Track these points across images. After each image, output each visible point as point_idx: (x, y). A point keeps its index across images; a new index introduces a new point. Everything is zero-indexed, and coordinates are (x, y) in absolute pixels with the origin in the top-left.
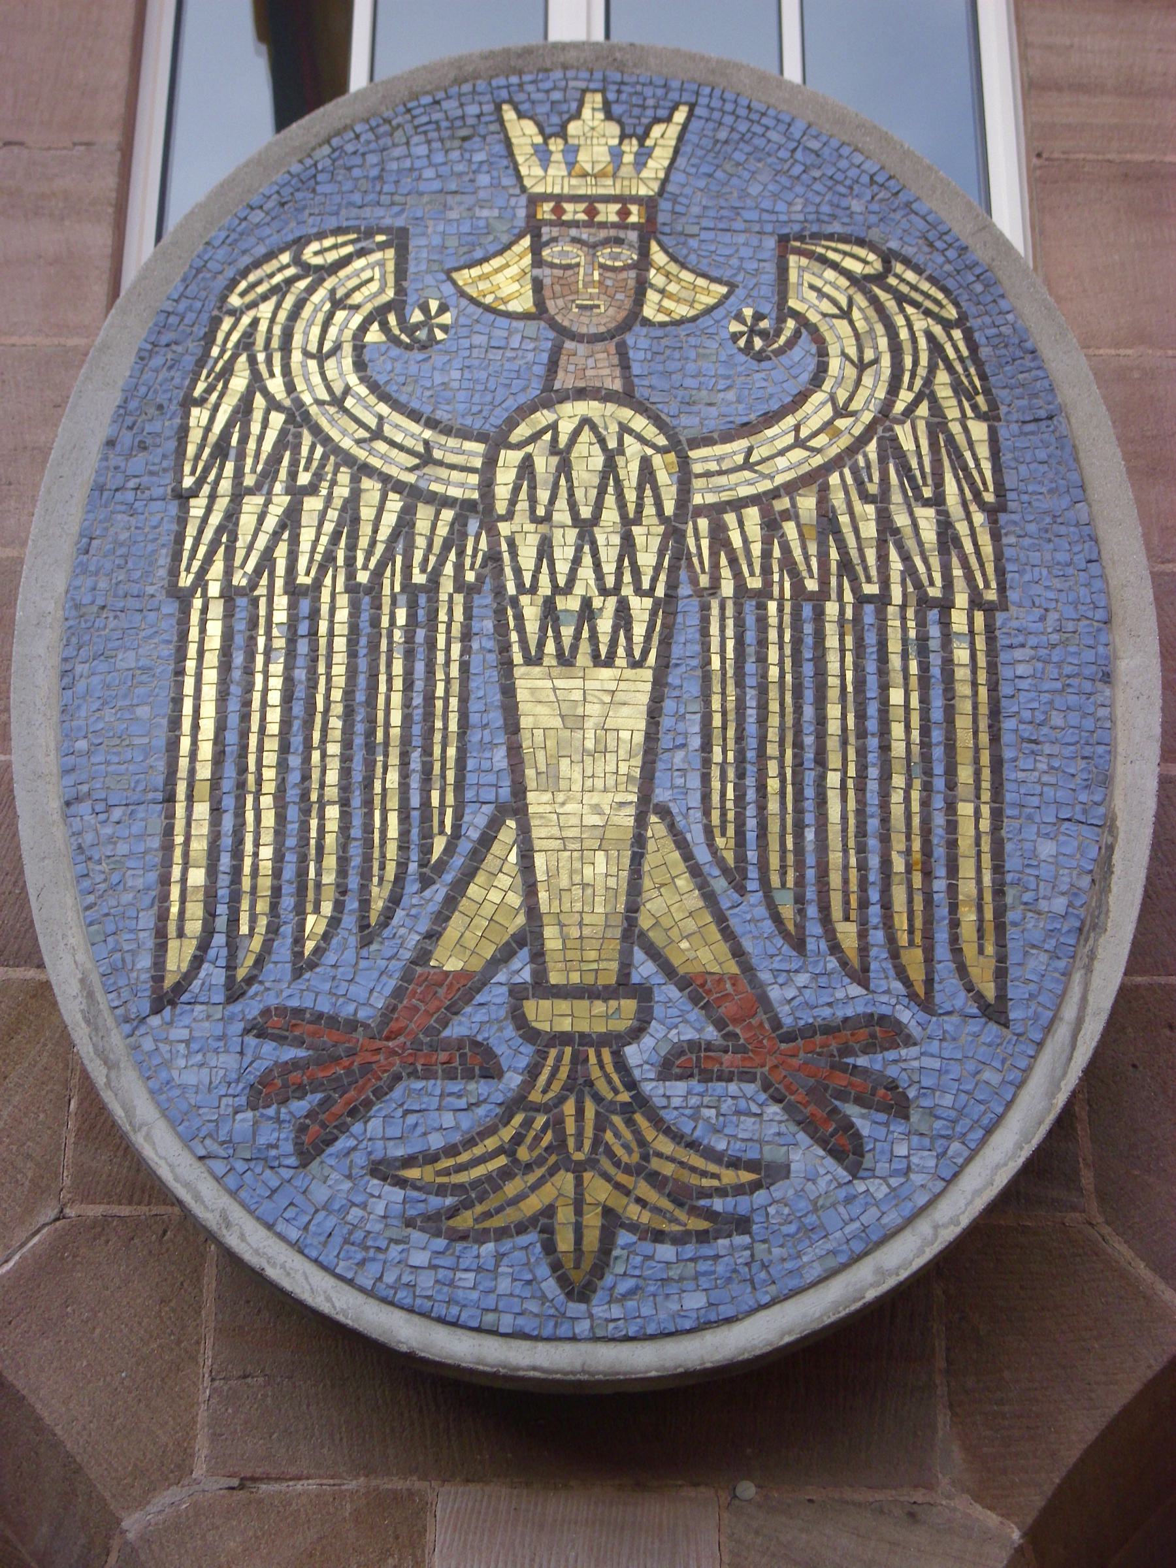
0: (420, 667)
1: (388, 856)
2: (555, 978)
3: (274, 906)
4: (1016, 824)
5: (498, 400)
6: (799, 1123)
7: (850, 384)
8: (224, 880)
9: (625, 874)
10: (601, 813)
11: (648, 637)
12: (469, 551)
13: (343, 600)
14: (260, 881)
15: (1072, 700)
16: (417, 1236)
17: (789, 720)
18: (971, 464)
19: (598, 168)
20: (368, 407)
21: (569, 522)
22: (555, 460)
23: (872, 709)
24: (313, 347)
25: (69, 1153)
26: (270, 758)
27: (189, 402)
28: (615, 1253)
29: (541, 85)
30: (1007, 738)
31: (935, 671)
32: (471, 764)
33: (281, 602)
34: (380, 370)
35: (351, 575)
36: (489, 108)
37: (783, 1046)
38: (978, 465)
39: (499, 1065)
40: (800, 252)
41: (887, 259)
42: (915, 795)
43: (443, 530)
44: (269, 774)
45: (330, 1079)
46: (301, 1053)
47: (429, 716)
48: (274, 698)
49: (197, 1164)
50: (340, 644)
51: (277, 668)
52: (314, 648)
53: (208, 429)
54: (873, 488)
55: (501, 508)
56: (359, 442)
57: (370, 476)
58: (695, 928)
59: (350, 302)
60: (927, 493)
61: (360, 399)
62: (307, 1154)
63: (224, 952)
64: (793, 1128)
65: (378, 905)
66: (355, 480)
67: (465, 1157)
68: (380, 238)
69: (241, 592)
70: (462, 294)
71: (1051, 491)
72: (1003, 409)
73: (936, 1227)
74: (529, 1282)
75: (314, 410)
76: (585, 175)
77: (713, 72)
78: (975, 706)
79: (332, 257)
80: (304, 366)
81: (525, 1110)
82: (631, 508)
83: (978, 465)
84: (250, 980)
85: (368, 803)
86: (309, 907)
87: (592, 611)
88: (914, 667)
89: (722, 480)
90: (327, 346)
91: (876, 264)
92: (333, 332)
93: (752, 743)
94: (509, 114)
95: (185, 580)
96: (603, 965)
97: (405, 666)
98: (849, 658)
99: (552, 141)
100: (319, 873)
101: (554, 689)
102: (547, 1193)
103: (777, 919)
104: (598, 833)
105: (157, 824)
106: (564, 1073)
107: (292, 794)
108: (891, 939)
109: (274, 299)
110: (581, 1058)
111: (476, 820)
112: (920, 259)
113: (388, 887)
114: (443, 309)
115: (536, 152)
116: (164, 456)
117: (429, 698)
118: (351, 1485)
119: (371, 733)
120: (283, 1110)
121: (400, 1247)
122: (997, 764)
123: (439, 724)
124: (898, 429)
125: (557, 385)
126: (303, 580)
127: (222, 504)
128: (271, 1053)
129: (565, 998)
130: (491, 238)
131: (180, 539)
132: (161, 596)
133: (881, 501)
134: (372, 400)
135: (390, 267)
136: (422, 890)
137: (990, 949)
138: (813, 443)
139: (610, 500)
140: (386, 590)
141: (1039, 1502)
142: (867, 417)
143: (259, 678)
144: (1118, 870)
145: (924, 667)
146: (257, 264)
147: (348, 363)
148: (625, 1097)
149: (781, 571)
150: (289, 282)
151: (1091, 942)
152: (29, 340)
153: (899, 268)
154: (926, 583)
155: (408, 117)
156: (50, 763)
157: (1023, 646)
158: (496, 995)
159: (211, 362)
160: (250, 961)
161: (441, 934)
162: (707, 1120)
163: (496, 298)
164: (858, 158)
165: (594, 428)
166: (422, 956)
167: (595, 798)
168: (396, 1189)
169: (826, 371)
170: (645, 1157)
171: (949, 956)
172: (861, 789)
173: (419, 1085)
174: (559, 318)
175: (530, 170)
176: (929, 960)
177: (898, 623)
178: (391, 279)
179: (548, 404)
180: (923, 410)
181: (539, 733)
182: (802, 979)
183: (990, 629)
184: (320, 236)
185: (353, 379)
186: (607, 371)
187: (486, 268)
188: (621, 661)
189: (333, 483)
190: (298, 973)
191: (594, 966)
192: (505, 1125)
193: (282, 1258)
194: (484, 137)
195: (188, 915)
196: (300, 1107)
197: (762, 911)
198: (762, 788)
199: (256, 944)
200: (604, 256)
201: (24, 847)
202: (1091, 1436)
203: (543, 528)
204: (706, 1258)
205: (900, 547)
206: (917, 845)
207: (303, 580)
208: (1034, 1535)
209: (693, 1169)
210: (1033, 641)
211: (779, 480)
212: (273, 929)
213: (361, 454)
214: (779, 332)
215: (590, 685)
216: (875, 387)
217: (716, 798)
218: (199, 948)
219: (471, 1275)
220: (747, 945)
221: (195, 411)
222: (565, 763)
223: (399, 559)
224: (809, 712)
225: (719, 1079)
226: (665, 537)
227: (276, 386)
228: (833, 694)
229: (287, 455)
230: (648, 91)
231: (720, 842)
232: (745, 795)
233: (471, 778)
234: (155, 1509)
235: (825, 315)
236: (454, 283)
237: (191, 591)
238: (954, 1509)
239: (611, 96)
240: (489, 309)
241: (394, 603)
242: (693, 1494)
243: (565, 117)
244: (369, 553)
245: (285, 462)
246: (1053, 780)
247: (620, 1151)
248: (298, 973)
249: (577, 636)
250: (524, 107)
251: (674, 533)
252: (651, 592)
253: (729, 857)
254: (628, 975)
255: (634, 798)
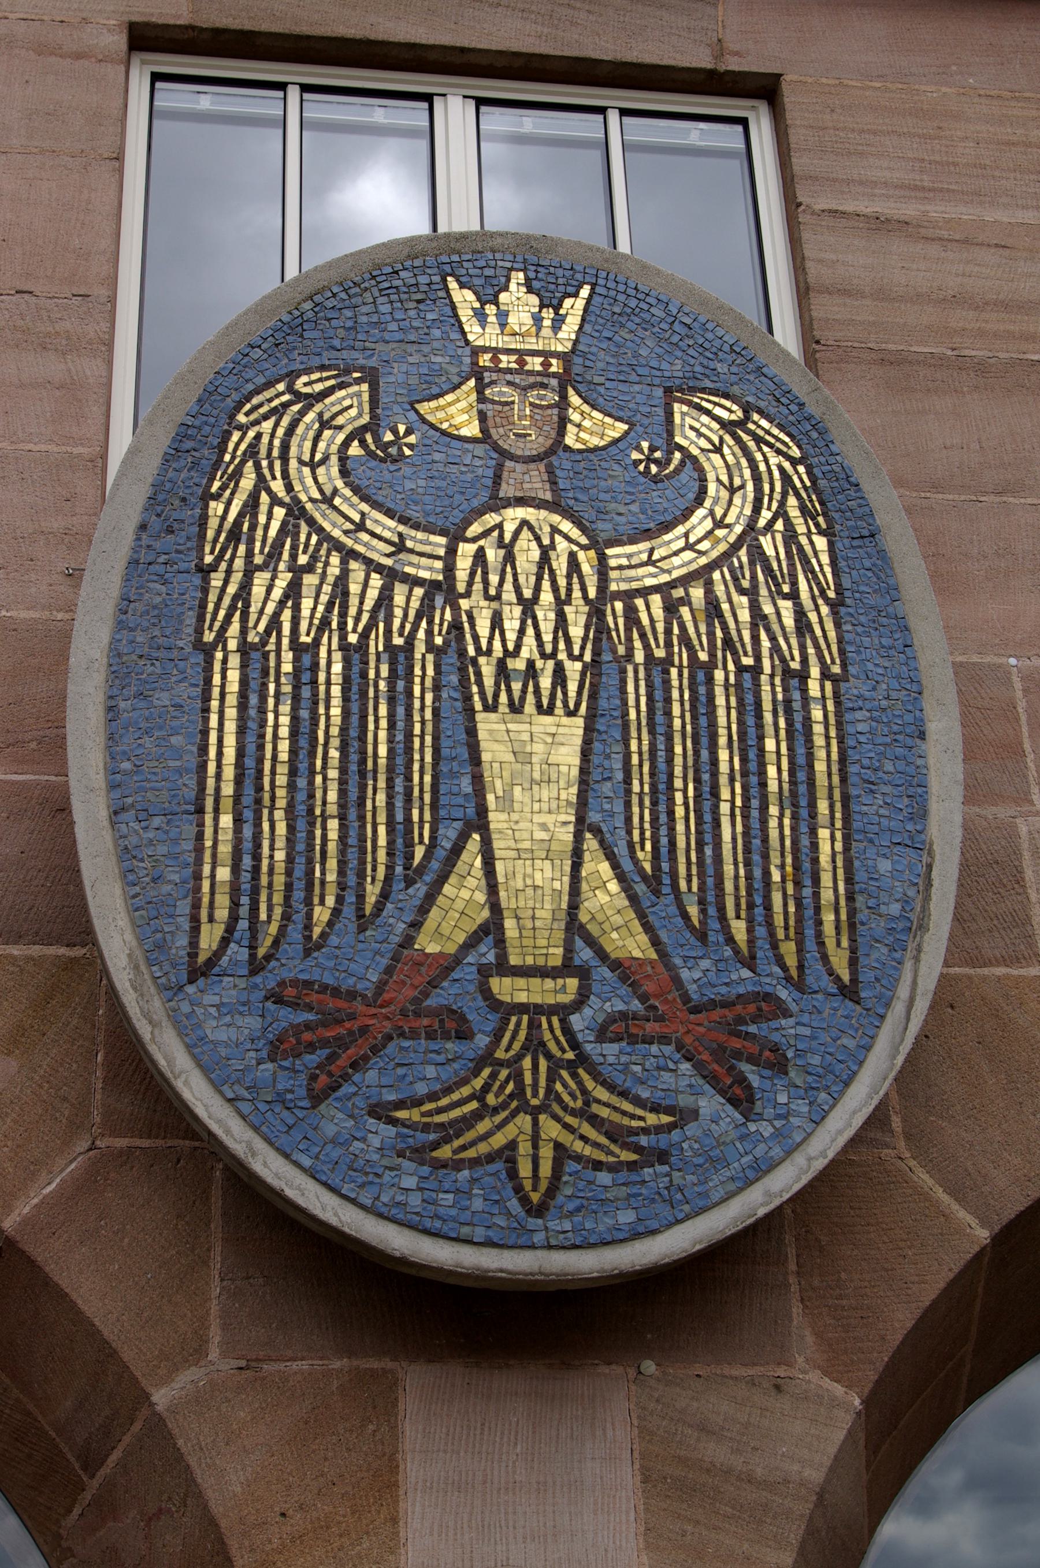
0: (401, 711)
1: (379, 860)
2: (514, 960)
3: (287, 898)
4: (861, 845)
5: (456, 503)
6: (704, 1077)
7: (724, 502)
8: (246, 877)
9: (566, 879)
10: (547, 830)
11: (580, 693)
12: (437, 621)
13: (337, 656)
14: (276, 878)
15: (899, 751)
16: (406, 1164)
17: (690, 762)
18: (817, 568)
19: (524, 329)
20: (352, 506)
21: (515, 601)
22: (502, 552)
23: (752, 755)
24: (306, 457)
25: (98, 1096)
26: (282, 780)
27: (207, 497)
28: (565, 1178)
29: (476, 263)
30: (853, 779)
31: (798, 726)
32: (443, 788)
33: (288, 656)
34: (360, 474)
35: (343, 637)
36: (437, 279)
37: (692, 1016)
38: (822, 570)
39: (470, 1029)
40: (682, 402)
41: (747, 409)
42: (787, 822)
43: (415, 604)
44: (281, 793)
45: (335, 1038)
46: (310, 1017)
47: (409, 750)
48: (284, 732)
49: (227, 1105)
50: (336, 691)
51: (285, 708)
52: (315, 694)
53: (223, 518)
54: (746, 584)
55: (461, 588)
56: (346, 532)
57: (356, 560)
58: (622, 922)
59: (334, 423)
60: (786, 589)
61: (346, 499)
62: (317, 1099)
63: (248, 934)
64: (701, 1082)
65: (371, 899)
66: (344, 562)
67: (444, 1102)
68: (356, 375)
69: (254, 647)
70: (424, 421)
71: (875, 591)
72: (838, 527)
73: (810, 1159)
74: (497, 1202)
75: (309, 506)
76: (515, 334)
77: (607, 261)
78: (829, 755)
79: (318, 387)
80: (300, 472)
81: (491, 1065)
82: (563, 592)
83: (822, 570)
84: (268, 958)
85: (362, 818)
86: (316, 900)
87: (535, 671)
88: (782, 723)
89: (632, 573)
90: (318, 457)
91: (738, 414)
92: (322, 446)
93: (663, 777)
94: (452, 284)
95: (209, 637)
96: (551, 950)
97: (388, 710)
98: (734, 714)
99: (487, 306)
100: (323, 873)
101: (508, 731)
102: (510, 1131)
103: (685, 916)
104: (546, 845)
105: (192, 830)
106: (522, 1035)
107: (301, 809)
108: (772, 934)
109: (273, 419)
110: (536, 1024)
111: (449, 833)
112: (772, 411)
113: (379, 885)
114: (409, 432)
115: (475, 314)
116: (189, 539)
117: (409, 735)
118: (337, 1364)
119: (363, 761)
120: (297, 1062)
121: (393, 1174)
122: (846, 799)
123: (417, 757)
124: (761, 538)
125: (501, 495)
126: (304, 639)
127: (237, 577)
128: (287, 1017)
129: (522, 976)
130: (444, 379)
131: (203, 605)
132: (189, 649)
133: (752, 593)
134: (355, 500)
135: (366, 397)
136: (407, 888)
137: (845, 943)
138: (699, 547)
139: (546, 585)
140: (372, 650)
141: (873, 1376)
142: (738, 529)
143: (271, 717)
144: (936, 882)
145: (790, 723)
146: (258, 391)
147: (335, 471)
148: (570, 1055)
149: (680, 644)
150: (286, 405)
151: (918, 939)
152: (43, 447)
153: (756, 417)
154: (788, 658)
155: (373, 282)
156: (99, 780)
157: (861, 709)
158: (467, 972)
159: (224, 466)
160: (269, 941)
161: (422, 924)
162: (634, 1074)
163: (451, 425)
164: (720, 332)
165: (531, 528)
166: (408, 941)
167: (537, 819)
168: (390, 1127)
169: (706, 493)
170: (587, 1103)
171: (816, 948)
172: (745, 817)
173: (406, 1044)
174: (501, 442)
175: (473, 330)
176: (800, 950)
177: (768, 688)
178: (366, 408)
179: (496, 509)
180: (779, 525)
181: (496, 765)
182: (705, 964)
183: (836, 695)
184: (308, 371)
185: (339, 484)
186: (540, 485)
187: (442, 401)
188: (559, 709)
189: (327, 564)
190: (307, 953)
191: (544, 951)
192: (476, 1077)
193: (298, 1181)
194: (434, 301)
195: (217, 904)
196: (312, 1059)
197: (673, 910)
198: (671, 813)
199: (273, 929)
200: (533, 396)
201: (80, 847)
202: (909, 1325)
203: (495, 605)
204: (635, 1183)
205: (768, 630)
206: (789, 860)
207: (304, 639)
208: (866, 1402)
209: (624, 1113)
210: (868, 705)
211: (676, 574)
212: (286, 917)
213: (349, 542)
214: (669, 461)
215: (535, 729)
216: (743, 506)
217: (636, 820)
218: (226, 931)
219: (451, 1196)
220: (663, 935)
221: (213, 504)
222: (517, 790)
223: (381, 625)
224: (705, 754)
225: (644, 1042)
226: (589, 615)
227: (277, 486)
228: (723, 741)
229: (289, 541)
230: (560, 272)
231: (640, 855)
232: (658, 818)
233: (443, 800)
234: (178, 1386)
235: (703, 450)
236: (417, 412)
237: (214, 646)
238: (809, 1382)
239: (532, 275)
240: (444, 433)
241: (378, 660)
242: (607, 1371)
243: (497, 288)
244: (357, 619)
245: (287, 546)
246: (887, 813)
247: (566, 1098)
248: (307, 953)
249: (524, 691)
250: (463, 279)
251: (596, 611)
252: (580, 658)
253: (647, 867)
254: (571, 958)
255: (573, 819)
